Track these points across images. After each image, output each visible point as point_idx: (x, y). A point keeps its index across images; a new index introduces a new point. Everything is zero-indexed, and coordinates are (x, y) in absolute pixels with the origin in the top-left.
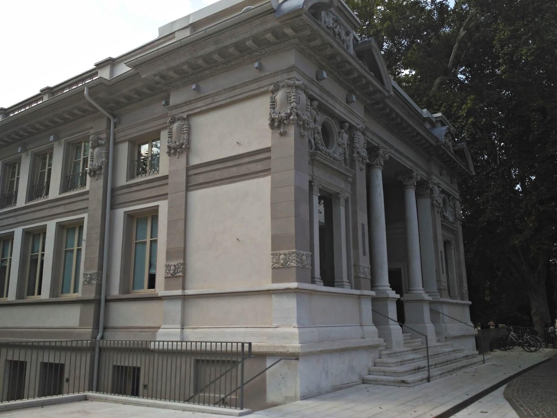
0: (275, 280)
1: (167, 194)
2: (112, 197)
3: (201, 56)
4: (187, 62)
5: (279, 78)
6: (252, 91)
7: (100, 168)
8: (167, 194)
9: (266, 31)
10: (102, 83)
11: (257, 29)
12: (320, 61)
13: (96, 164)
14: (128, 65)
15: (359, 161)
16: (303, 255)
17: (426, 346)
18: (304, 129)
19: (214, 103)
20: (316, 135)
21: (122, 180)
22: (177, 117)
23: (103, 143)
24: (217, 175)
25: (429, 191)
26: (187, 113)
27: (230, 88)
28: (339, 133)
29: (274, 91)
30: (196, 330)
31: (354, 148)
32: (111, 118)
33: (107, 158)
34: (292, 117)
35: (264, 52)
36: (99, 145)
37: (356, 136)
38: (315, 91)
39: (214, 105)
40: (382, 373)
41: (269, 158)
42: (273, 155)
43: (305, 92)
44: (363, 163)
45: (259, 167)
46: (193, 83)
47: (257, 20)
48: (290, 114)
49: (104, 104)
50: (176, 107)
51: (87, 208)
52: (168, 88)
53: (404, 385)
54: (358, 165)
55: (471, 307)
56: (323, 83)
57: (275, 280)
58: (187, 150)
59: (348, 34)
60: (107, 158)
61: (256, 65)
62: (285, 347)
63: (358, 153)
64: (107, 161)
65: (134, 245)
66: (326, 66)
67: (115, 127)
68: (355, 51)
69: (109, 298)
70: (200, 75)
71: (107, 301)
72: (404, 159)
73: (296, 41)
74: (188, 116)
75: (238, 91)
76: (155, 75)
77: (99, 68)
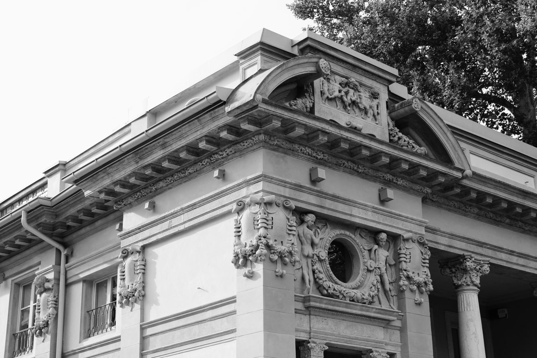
4: (133, 174)
5: (243, 192)
7: (47, 324)
9: (221, 129)
10: (41, 205)
11: (210, 126)
12: (314, 154)
13: (42, 317)
15: (412, 291)
18: (285, 264)
19: (171, 228)
20: (318, 266)
21: (74, 343)
22: (130, 248)
23: (50, 286)
26: (141, 244)
28: (370, 251)
31: (401, 270)
32: (61, 248)
33: (56, 309)
34: (258, 252)
35: (225, 155)
36: (46, 290)
37: (403, 251)
38: (308, 200)
44: (421, 293)
46: (146, 200)
47: (206, 115)
48: (257, 247)
49: (50, 230)
50: (129, 234)
52: (119, 207)
54: (409, 299)
56: (324, 187)
58: (141, 298)
59: (375, 96)
60: (56, 309)
61: (216, 173)
63: (408, 278)
64: (55, 312)
66: (326, 158)
67: (67, 262)
68: (392, 119)
70: (154, 189)
73: (262, 137)
74: (144, 247)
76: (100, 192)
77: (49, 176)
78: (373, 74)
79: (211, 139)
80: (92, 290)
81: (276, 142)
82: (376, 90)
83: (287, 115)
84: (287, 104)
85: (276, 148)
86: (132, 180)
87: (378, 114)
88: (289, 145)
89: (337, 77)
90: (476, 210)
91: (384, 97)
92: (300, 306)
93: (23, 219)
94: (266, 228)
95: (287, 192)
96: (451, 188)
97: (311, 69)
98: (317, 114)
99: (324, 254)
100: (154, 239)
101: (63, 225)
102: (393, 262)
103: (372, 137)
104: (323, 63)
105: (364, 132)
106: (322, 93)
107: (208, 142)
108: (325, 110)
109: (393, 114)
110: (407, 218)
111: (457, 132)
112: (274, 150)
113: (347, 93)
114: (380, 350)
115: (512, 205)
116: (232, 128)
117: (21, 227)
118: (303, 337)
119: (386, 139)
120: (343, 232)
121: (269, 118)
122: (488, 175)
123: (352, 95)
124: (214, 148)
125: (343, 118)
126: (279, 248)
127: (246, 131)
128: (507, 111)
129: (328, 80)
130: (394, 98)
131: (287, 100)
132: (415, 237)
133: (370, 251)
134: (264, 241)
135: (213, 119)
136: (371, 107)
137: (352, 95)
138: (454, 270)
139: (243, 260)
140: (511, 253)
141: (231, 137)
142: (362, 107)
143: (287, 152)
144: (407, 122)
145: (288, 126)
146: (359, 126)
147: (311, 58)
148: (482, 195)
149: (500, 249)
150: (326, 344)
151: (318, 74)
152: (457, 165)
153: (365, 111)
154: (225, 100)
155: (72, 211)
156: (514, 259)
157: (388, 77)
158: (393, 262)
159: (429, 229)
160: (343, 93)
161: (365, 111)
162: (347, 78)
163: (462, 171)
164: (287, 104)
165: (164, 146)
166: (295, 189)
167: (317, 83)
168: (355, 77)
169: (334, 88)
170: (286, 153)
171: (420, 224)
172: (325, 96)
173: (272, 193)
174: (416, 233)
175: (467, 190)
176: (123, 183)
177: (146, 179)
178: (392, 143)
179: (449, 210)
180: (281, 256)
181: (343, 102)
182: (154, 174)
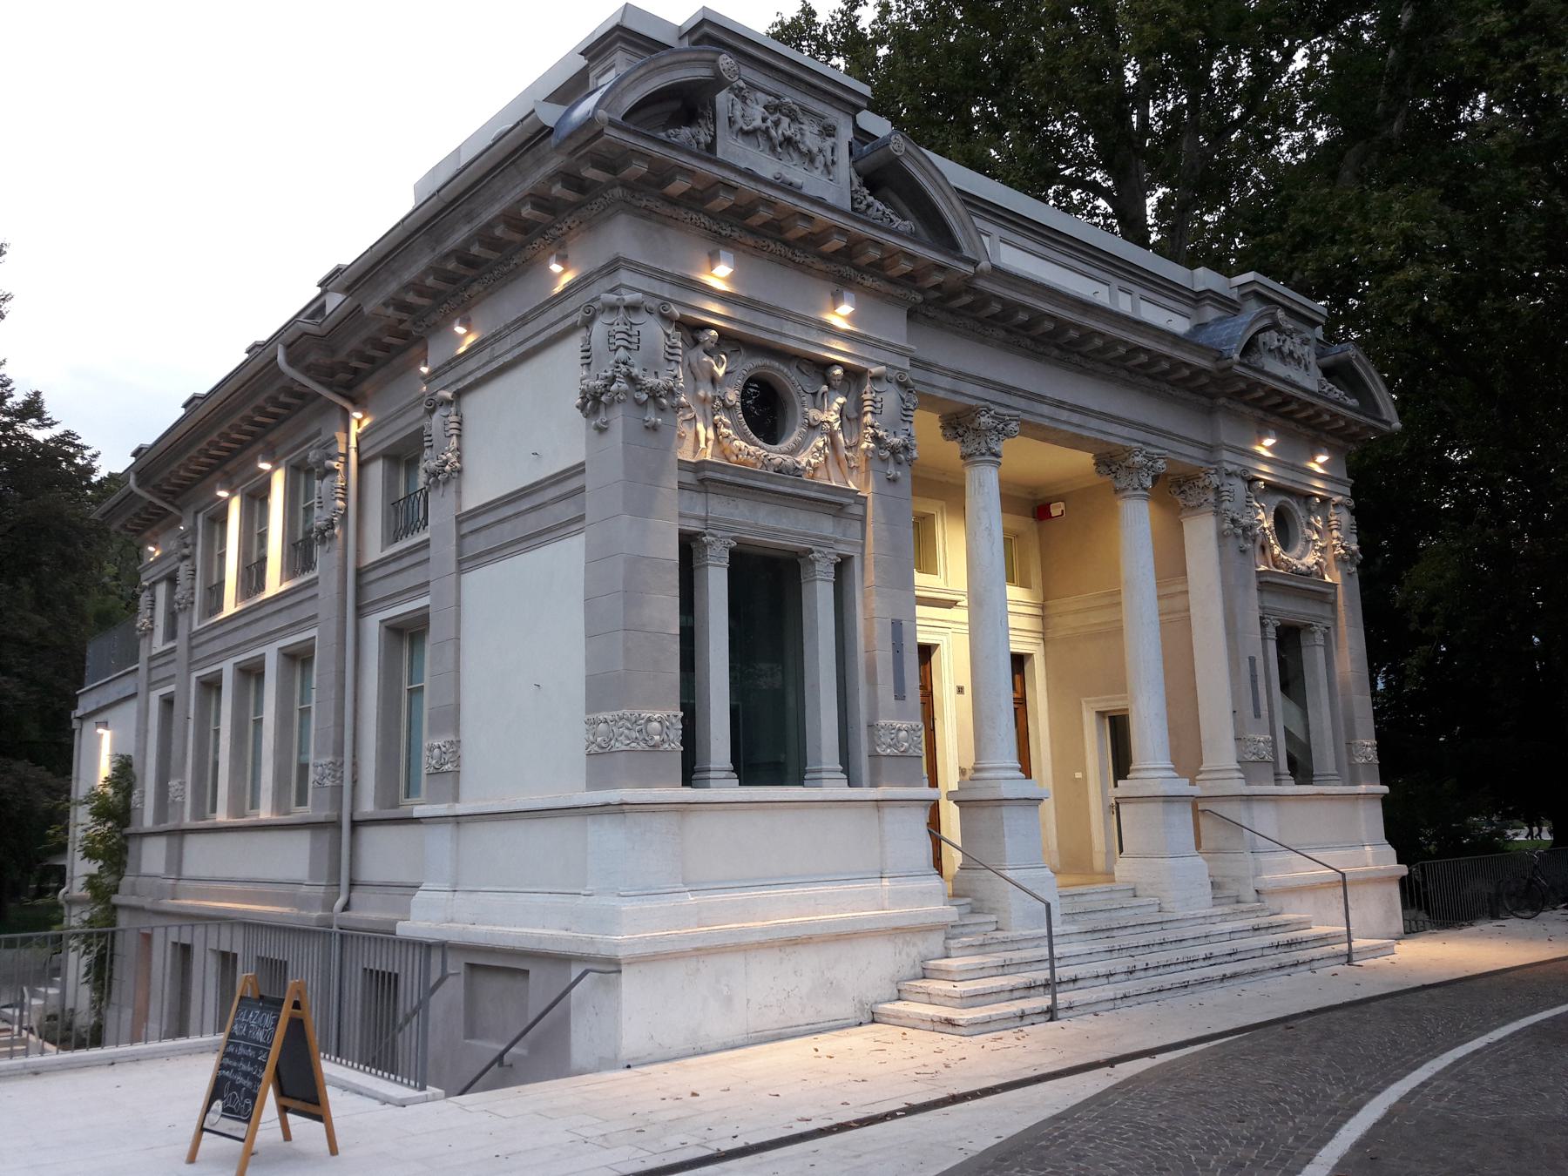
0: (593, 783)
1: (427, 583)
2: (359, 588)
3: (453, 251)
6: (553, 325)
8: (427, 583)
11: (535, 176)
12: (715, 228)
14: (336, 290)
16: (649, 720)
17: (1044, 931)
20: (722, 417)
24: (507, 532)
25: (1211, 497)
27: (516, 321)
28: (814, 394)
29: (588, 323)
30: (474, 896)
34: (614, 387)
39: (495, 365)
40: (925, 998)
41: (582, 489)
42: (588, 480)
43: (666, 318)
45: (566, 511)
48: (613, 380)
49: (326, 375)
51: (315, 616)
53: (950, 1029)
55: (1386, 801)
57: (593, 783)
59: (829, 131)
62: (592, 941)
65: (405, 695)
68: (859, 174)
69: (357, 817)
71: (355, 825)
72: (1094, 423)
73: (618, 192)
75: (531, 328)
78: (826, 92)
79: (540, 200)
80: (398, 474)
81: (644, 203)
82: (831, 121)
83: (657, 150)
84: (662, 135)
85: (647, 214)
86: (430, 281)
87: (833, 162)
88: (668, 210)
89: (759, 94)
90: (1002, 334)
91: (846, 134)
92: (689, 478)
93: (281, 358)
94: (626, 348)
95: (666, 291)
96: (955, 295)
97: (703, 73)
98: (719, 155)
99: (733, 396)
100: (470, 380)
101: (345, 366)
102: (854, 415)
103: (818, 202)
104: (725, 61)
105: (805, 191)
106: (731, 121)
107: (536, 206)
108: (732, 149)
109: (860, 164)
110: (879, 341)
111: (972, 202)
112: (642, 217)
113: (777, 124)
114: (826, 551)
115: (1062, 325)
116: (570, 178)
117: (281, 373)
118: (694, 526)
119: (847, 206)
120: (767, 362)
121: (630, 154)
122: (1014, 271)
123: (786, 128)
124: (548, 218)
125: (768, 166)
126: (650, 380)
127: (595, 183)
128: (1101, 203)
129: (744, 100)
130: (862, 135)
131: (665, 128)
132: (893, 374)
133: (814, 394)
134: (623, 369)
135: (539, 162)
136: (820, 151)
137: (786, 128)
138: (960, 431)
139: (593, 403)
140: (1060, 404)
141: (571, 196)
142: (805, 150)
143: (666, 222)
144: (880, 177)
145: (661, 175)
146: (797, 180)
147: (707, 51)
148: (1011, 308)
149: (1041, 399)
150: (733, 538)
151: (718, 83)
152: (967, 253)
153: (810, 157)
154: (551, 124)
155: (354, 343)
156: (1064, 415)
157: (852, 99)
158: (854, 415)
159: (916, 362)
160: (769, 123)
161: (810, 157)
162: (777, 97)
163: (975, 263)
164: (662, 135)
165: (469, 217)
166: (679, 286)
167: (723, 98)
168: (791, 97)
169: (756, 115)
170: (665, 224)
171: (902, 352)
172: (737, 127)
173: (639, 291)
174: (894, 368)
175: (985, 299)
176: (416, 287)
177: (452, 279)
178: (855, 213)
179: (957, 333)
180: (654, 395)
181: (770, 138)
182: (462, 270)
